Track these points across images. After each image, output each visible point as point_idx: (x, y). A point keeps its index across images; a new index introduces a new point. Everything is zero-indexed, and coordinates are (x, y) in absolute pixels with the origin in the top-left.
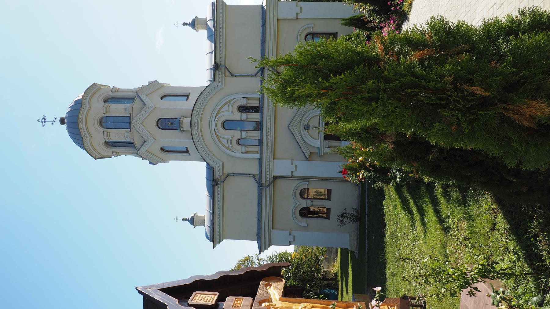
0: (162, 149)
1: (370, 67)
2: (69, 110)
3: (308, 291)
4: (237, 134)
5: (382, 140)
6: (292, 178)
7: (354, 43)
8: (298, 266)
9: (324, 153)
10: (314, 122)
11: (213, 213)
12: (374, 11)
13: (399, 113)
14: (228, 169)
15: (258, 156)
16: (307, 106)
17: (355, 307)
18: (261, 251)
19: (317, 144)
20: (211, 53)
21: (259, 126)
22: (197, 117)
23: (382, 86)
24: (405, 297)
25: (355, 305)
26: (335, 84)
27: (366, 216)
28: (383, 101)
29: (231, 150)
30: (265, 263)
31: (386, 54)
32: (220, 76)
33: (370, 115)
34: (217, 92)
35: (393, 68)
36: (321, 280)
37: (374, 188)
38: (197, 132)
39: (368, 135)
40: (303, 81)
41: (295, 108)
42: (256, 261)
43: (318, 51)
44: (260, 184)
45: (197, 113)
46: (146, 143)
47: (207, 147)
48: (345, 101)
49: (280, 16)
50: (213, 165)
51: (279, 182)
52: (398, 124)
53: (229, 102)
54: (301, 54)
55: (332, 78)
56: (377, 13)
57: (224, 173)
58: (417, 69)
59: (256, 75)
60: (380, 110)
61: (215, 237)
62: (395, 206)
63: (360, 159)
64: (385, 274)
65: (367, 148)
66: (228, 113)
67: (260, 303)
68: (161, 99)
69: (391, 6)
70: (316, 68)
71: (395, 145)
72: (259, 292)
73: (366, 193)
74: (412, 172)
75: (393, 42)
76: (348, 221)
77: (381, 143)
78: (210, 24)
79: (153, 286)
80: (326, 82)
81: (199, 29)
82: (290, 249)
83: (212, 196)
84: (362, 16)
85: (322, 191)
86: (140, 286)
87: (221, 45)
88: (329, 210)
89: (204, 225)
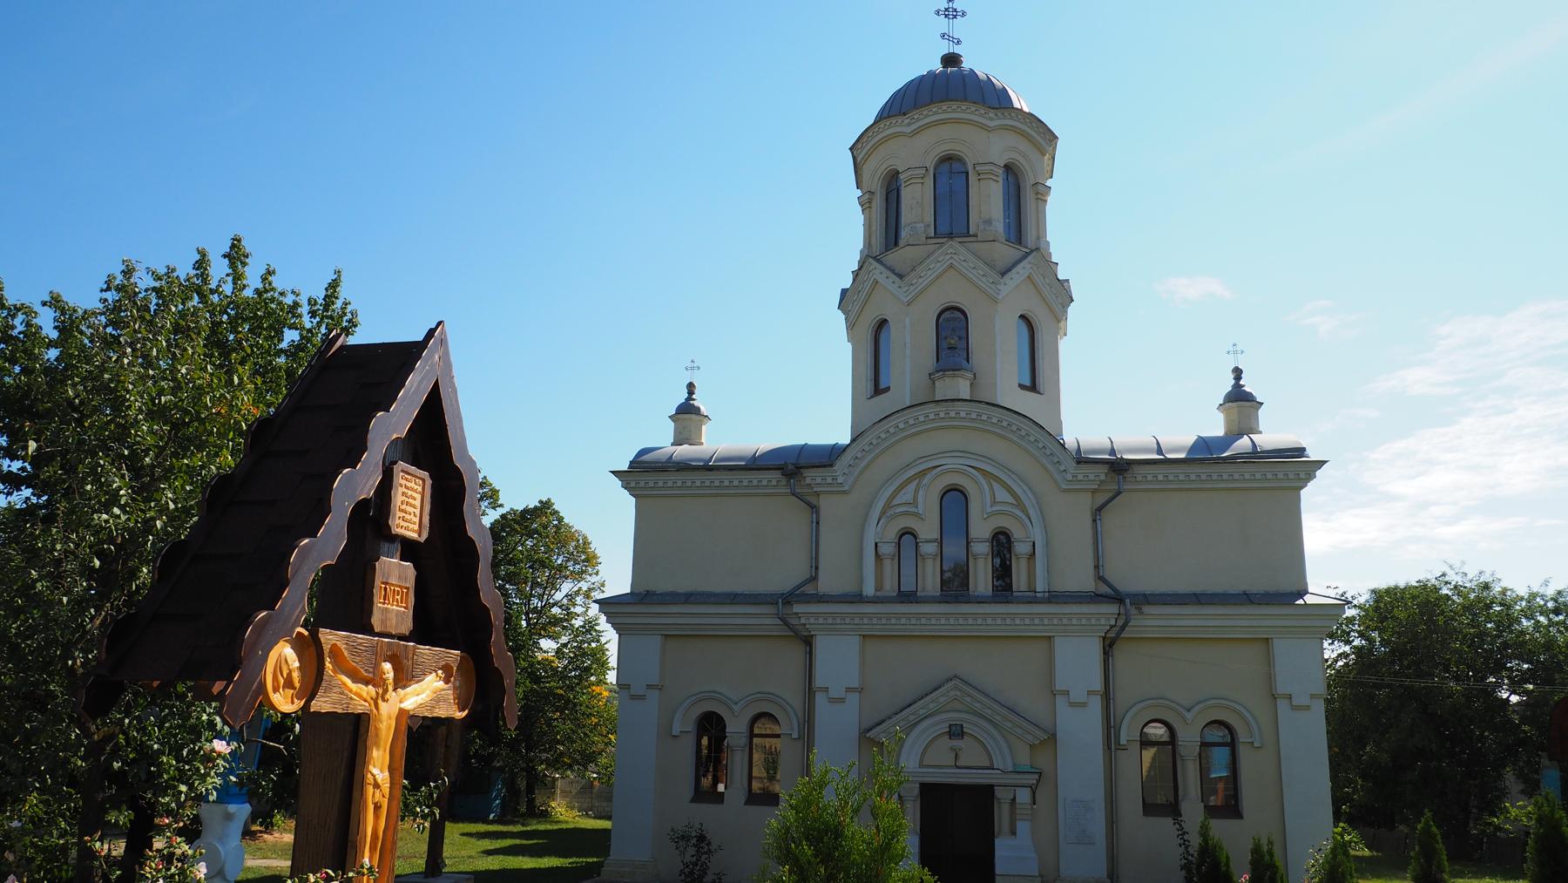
0: (882, 323)
2: (982, 76)
4: (928, 529)
6: (810, 691)
15: (869, 589)
18: (604, 604)
19: (909, 761)
20: (1160, 451)
22: (974, 416)
29: (883, 513)
32: (1091, 477)
34: (1047, 470)
36: (531, 772)
38: (932, 416)
44: (789, 598)
46: (897, 279)
47: (888, 448)
49: (1280, 646)
51: (796, 653)
53: (1020, 504)
57: (817, 494)
59: (1101, 579)
61: (643, 475)
67: (394, 660)
68: (1022, 317)
72: (424, 650)
76: (688, 858)
78: (1243, 443)
79: (448, 366)
83: (757, 464)
86: (452, 333)
89: (676, 443)
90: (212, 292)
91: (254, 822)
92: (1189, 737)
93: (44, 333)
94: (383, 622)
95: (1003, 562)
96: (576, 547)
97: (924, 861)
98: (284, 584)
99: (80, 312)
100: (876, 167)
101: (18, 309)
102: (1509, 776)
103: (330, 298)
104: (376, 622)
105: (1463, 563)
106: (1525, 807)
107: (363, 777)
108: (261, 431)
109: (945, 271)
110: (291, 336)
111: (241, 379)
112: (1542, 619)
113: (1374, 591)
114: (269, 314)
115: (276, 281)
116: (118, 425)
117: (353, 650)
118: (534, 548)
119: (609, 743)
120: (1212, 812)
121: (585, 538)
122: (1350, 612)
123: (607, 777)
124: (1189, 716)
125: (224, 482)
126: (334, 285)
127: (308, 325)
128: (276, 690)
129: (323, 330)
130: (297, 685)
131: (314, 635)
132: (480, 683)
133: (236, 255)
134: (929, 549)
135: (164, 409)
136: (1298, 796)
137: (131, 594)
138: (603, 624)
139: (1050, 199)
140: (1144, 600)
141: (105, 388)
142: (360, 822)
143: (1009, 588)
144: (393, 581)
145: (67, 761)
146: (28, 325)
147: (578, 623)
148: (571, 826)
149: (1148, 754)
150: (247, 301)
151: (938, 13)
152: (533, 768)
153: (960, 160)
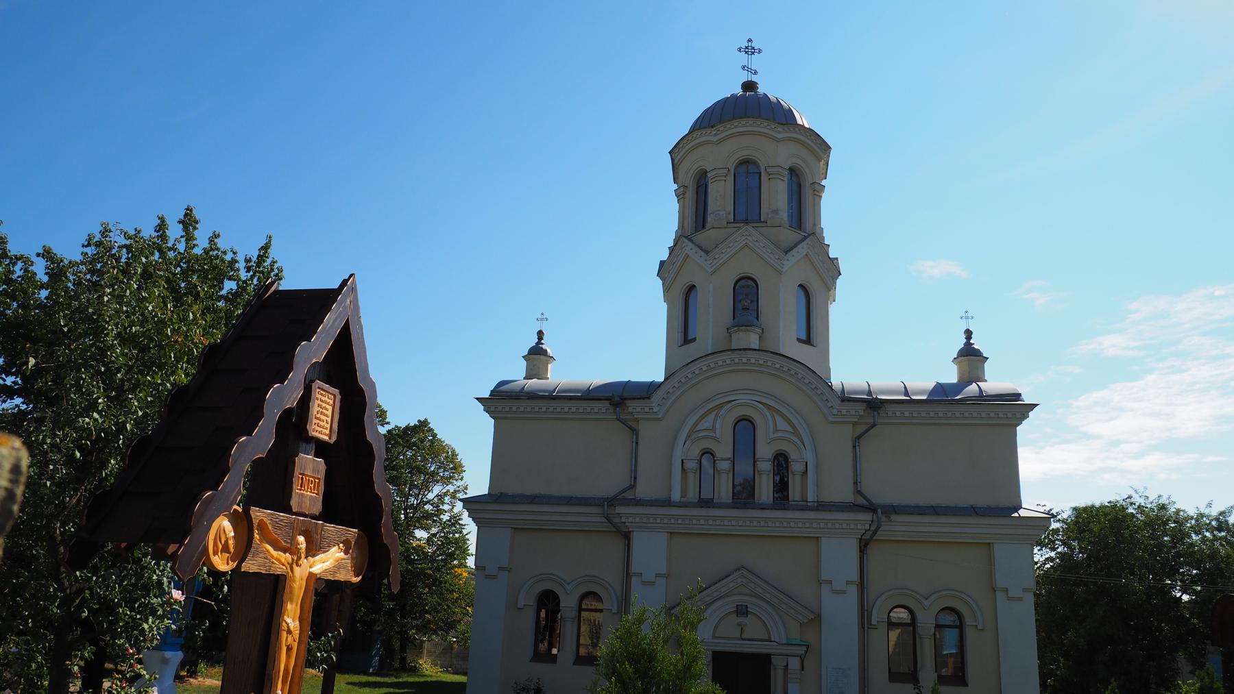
0: (692, 288)
4: (724, 451)
6: (627, 575)
15: (676, 496)
18: (467, 502)
20: (906, 393)
29: (689, 436)
32: (853, 412)
44: (612, 502)
49: (999, 551)
50: (656, 398)
53: (796, 432)
57: (637, 420)
59: (859, 493)
61: (501, 401)
72: (330, 527)
78: (973, 388)
90: (170, 249)
91: (182, 669)
92: (926, 620)
93: (38, 278)
94: (300, 504)
95: (782, 480)
96: (447, 457)
97: (715, 680)
98: (226, 470)
99: (66, 262)
100: (689, 167)
101: (18, 258)
102: (1181, 658)
103: (261, 258)
104: (294, 503)
106: (1193, 685)
107: (279, 625)
108: (211, 352)
109: (742, 248)
110: (229, 285)
111: (195, 315)
112: (1208, 534)
113: (1075, 509)
114: (215, 268)
115: (221, 243)
116: (98, 348)
117: (276, 524)
118: (414, 457)
119: (467, 614)
120: (943, 680)
121: (453, 451)
122: (1055, 525)
123: (464, 641)
124: (926, 603)
125: (180, 392)
126: (266, 248)
127: (244, 278)
128: (215, 553)
129: (255, 282)
130: (232, 550)
131: (246, 511)
132: (373, 554)
133: (189, 222)
135: (135, 336)
136: (1012, 655)
137: (101, 480)
138: (466, 519)
140: (893, 510)
141: (89, 319)
142: (275, 660)
143: (787, 498)
144: (308, 472)
145: (46, 608)
146: (26, 271)
147: (445, 517)
148: (434, 679)
149: (894, 634)
150: (197, 258)
151: (740, 50)
152: (406, 632)
153: (755, 163)
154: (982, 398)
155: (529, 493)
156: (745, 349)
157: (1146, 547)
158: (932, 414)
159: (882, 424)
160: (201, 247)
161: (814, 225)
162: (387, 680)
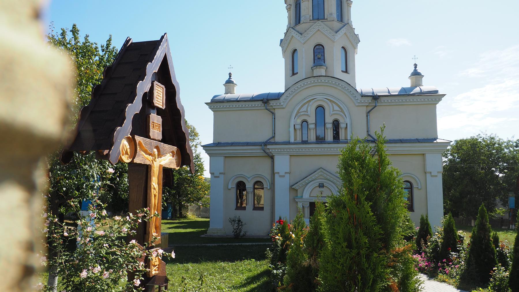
0: (295, 50)
1: (380, 240)
3: (168, 192)
4: (312, 120)
5: (312, 256)
6: (273, 174)
7: (403, 224)
8: (191, 182)
9: (297, 202)
10: (326, 192)
11: (237, 101)
12: (437, 246)
13: (338, 269)
14: (278, 113)
15: (292, 140)
16: (341, 181)
17: (157, 234)
18: (204, 147)
19: (306, 195)
20: (389, 92)
21: (320, 140)
22: (327, 81)
23: (363, 252)
24: (167, 280)
25: (158, 235)
26: (363, 206)
27: (240, 244)
28: (349, 252)
29: (296, 115)
30: (193, 151)
31: (394, 255)
32: (366, 101)
33: (335, 242)
34: (351, 99)
35: (380, 261)
36: (180, 203)
37: (266, 250)
38: (312, 82)
39: (316, 241)
40: (364, 176)
41: (338, 170)
42: (194, 143)
43: (394, 190)
44: (266, 144)
45: (330, 82)
46: (300, 35)
48: (347, 217)
49: (428, 156)
50: (282, 99)
51: (268, 161)
52: (328, 267)
53: (342, 111)
54: (391, 174)
55: (368, 203)
56: (435, 249)
57: (274, 109)
58: (381, 285)
59: (369, 135)
60: (339, 250)
61: (215, 104)
62: (250, 270)
63: (294, 236)
64: (187, 263)
65: (304, 241)
66: (332, 110)
67: (157, 147)
68: (342, 47)
69: (442, 262)
70: (377, 188)
71: (307, 267)
72: (166, 146)
73: (262, 243)
74: (282, 284)
75: (406, 263)
76: (235, 227)
77: (308, 254)
78: (417, 90)
79: (169, 49)
80: (364, 198)
81: (412, 79)
82: (207, 174)
83: (253, 100)
84: (430, 235)
85: (262, 202)
86: (169, 36)
87: (397, 101)
88: (244, 208)
89: (226, 93)
94: (153, 135)
102: (498, 199)
103: (108, 45)
105: (486, 131)
112: (511, 149)
113: (456, 141)
115: (90, 39)
119: (205, 194)
122: (449, 147)
126: (109, 40)
128: (123, 155)
133: (75, 31)
134: (312, 126)
139: (352, 6)
154: (421, 94)
155: (230, 142)
156: (320, 76)
157: (485, 155)
158: (400, 101)
159: (379, 106)
160: (81, 42)
161: (348, 20)
162: (175, 221)
